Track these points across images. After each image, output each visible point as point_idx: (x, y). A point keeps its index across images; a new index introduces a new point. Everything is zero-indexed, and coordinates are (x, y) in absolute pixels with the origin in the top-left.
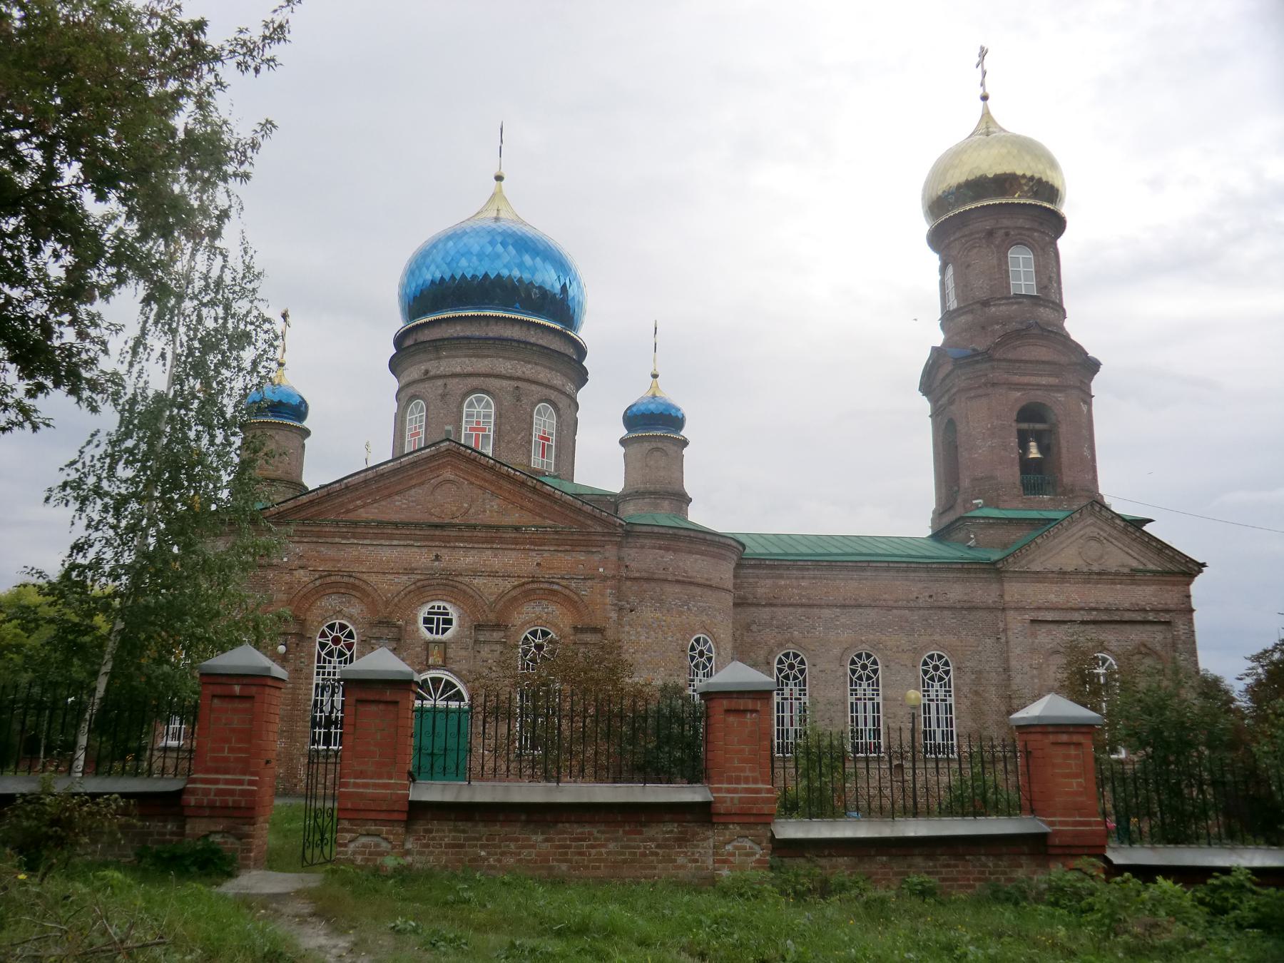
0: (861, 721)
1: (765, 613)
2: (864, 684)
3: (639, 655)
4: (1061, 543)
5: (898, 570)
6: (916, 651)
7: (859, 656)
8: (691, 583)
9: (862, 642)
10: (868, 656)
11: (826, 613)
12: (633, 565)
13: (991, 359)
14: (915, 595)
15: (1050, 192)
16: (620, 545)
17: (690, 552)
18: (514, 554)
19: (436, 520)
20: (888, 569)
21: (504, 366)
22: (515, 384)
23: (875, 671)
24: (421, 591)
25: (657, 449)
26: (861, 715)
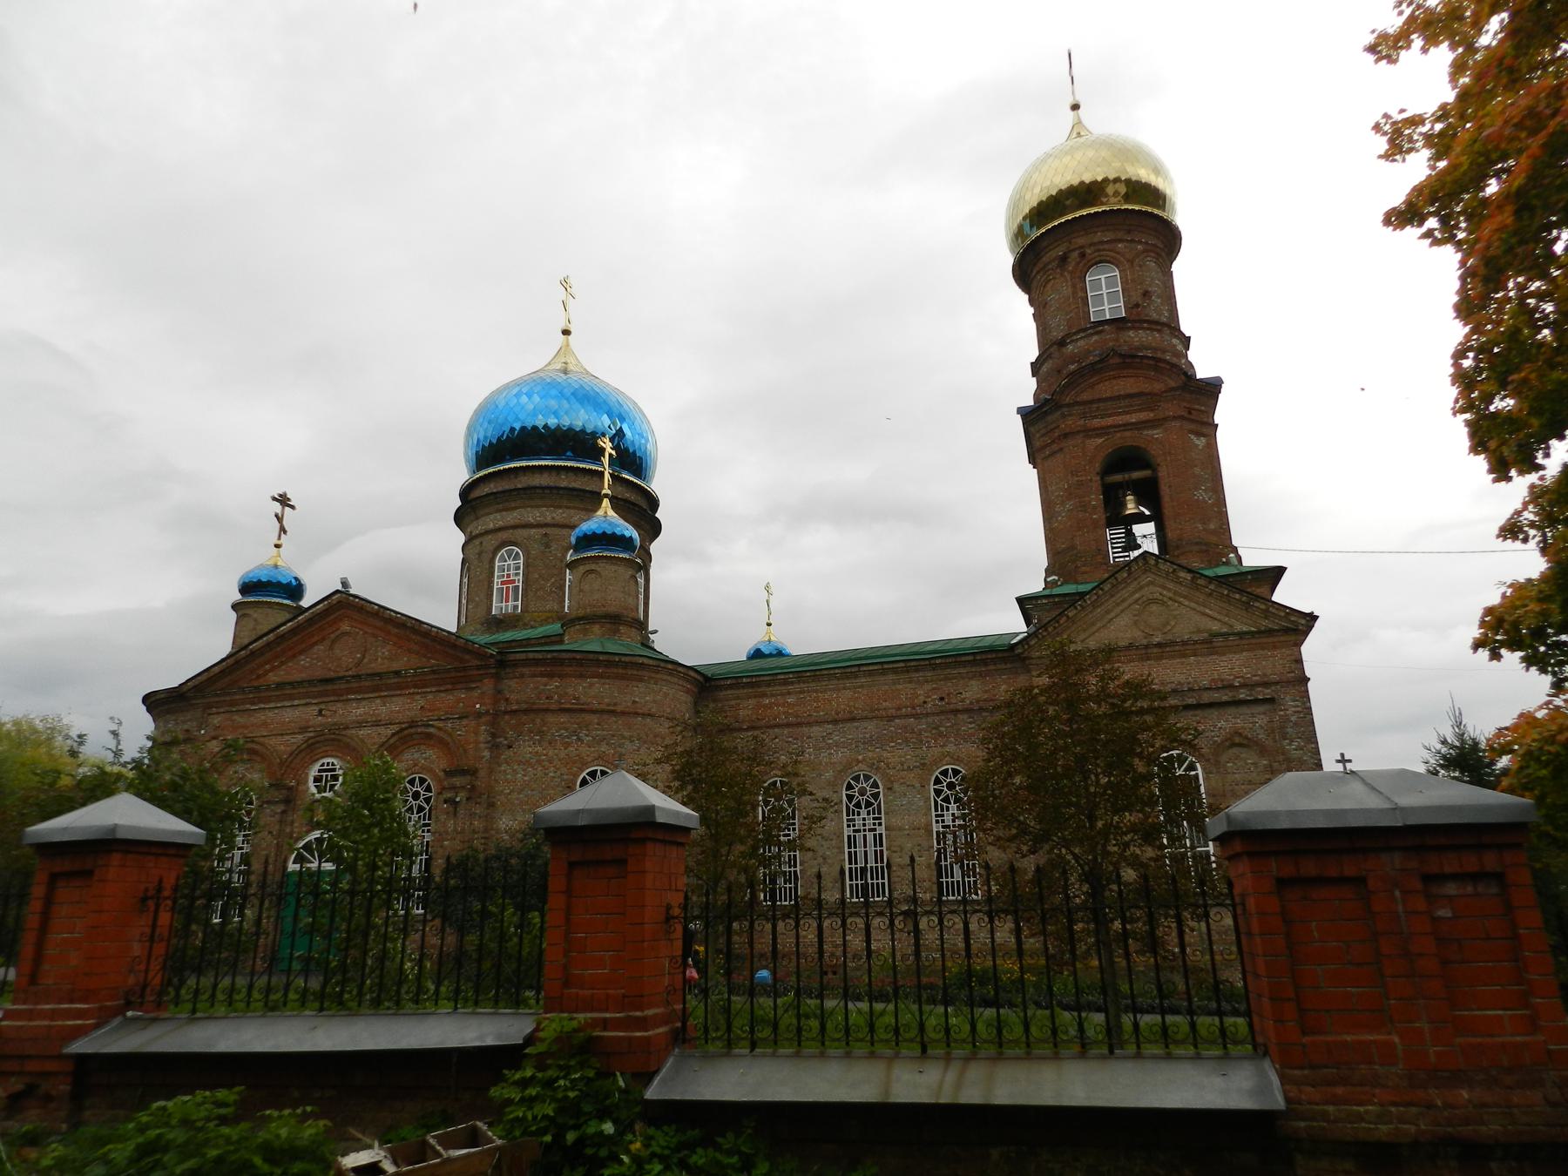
0: (861, 857)
2: (863, 812)
3: (515, 795)
4: (1108, 612)
5: (895, 671)
6: (925, 767)
7: (856, 779)
8: (582, 710)
9: (858, 762)
10: (867, 778)
11: (816, 731)
12: (513, 697)
13: (1058, 406)
14: (922, 698)
15: (1155, 196)
16: (498, 678)
17: (582, 676)
18: (400, 700)
19: (332, 674)
20: (884, 672)
21: (532, 515)
22: (543, 531)
23: (876, 796)
24: (311, 750)
25: (592, 571)
26: (860, 850)
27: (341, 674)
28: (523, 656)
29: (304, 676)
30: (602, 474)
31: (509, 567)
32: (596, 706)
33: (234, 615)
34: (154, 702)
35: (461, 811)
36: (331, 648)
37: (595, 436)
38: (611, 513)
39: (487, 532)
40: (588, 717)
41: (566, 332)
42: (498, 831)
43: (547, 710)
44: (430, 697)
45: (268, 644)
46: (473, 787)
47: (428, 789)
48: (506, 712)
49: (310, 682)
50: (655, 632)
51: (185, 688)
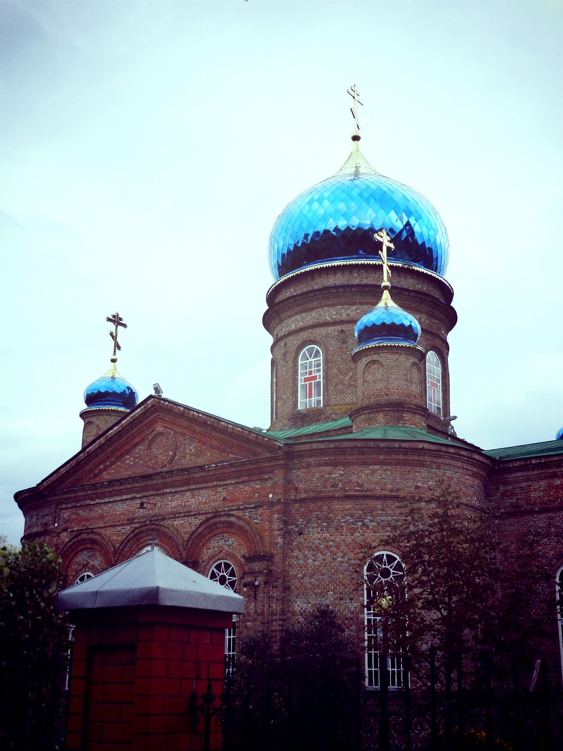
3: (307, 580)
8: (366, 497)
16: (287, 468)
17: (365, 464)
19: (151, 471)
22: (340, 328)
25: (374, 362)
27: (159, 470)
28: (308, 447)
30: (381, 267)
31: (311, 364)
32: (379, 492)
33: (81, 423)
35: (260, 595)
36: (149, 448)
37: (372, 231)
38: (391, 304)
39: (290, 334)
40: (372, 503)
41: (356, 138)
43: (332, 498)
44: (231, 488)
46: (270, 571)
47: (232, 574)
48: (295, 501)
49: (134, 479)
50: (455, 418)
51: (42, 488)
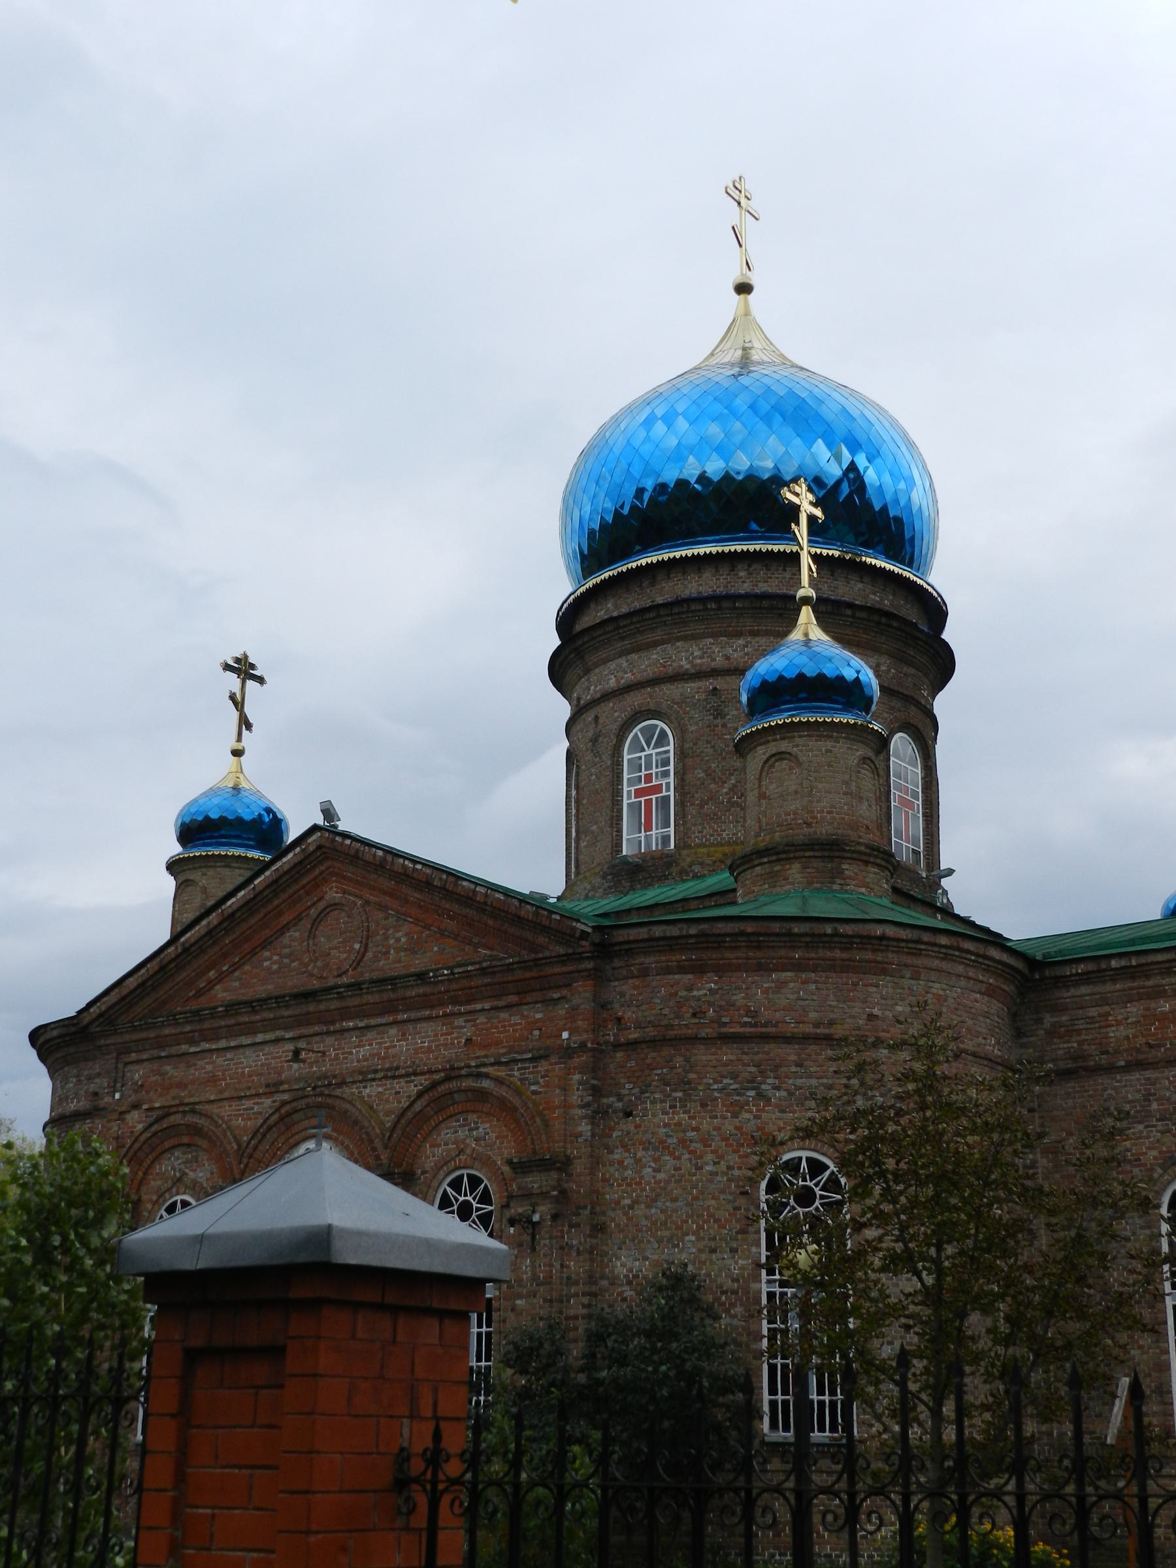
1: (1128, 1088)
3: (640, 1210)
8: (765, 1038)
16: (599, 978)
17: (761, 968)
18: (428, 1028)
19: (315, 984)
22: (709, 684)
25: (780, 756)
27: (331, 982)
28: (643, 933)
29: (269, 988)
30: (795, 558)
31: (649, 761)
32: (791, 1028)
34: (52, 1042)
35: (544, 1242)
36: (312, 935)
37: (778, 481)
38: (817, 634)
39: (606, 696)
40: (776, 1051)
42: (614, 1281)
43: (694, 1039)
44: (482, 1019)
45: (210, 933)
46: (563, 1192)
47: (485, 1198)
48: (617, 1046)
49: (279, 1000)
50: (950, 872)
51: (87, 1019)
